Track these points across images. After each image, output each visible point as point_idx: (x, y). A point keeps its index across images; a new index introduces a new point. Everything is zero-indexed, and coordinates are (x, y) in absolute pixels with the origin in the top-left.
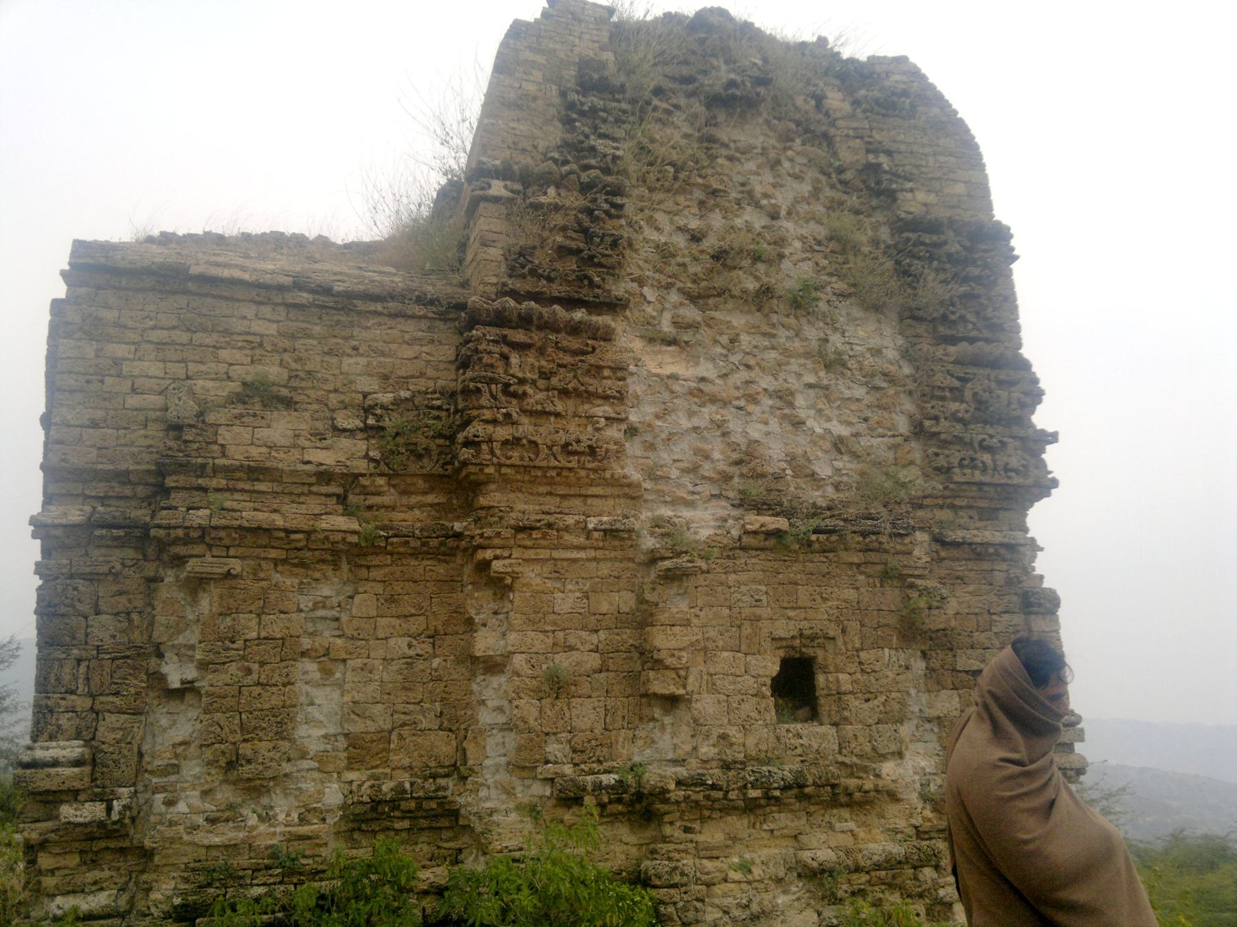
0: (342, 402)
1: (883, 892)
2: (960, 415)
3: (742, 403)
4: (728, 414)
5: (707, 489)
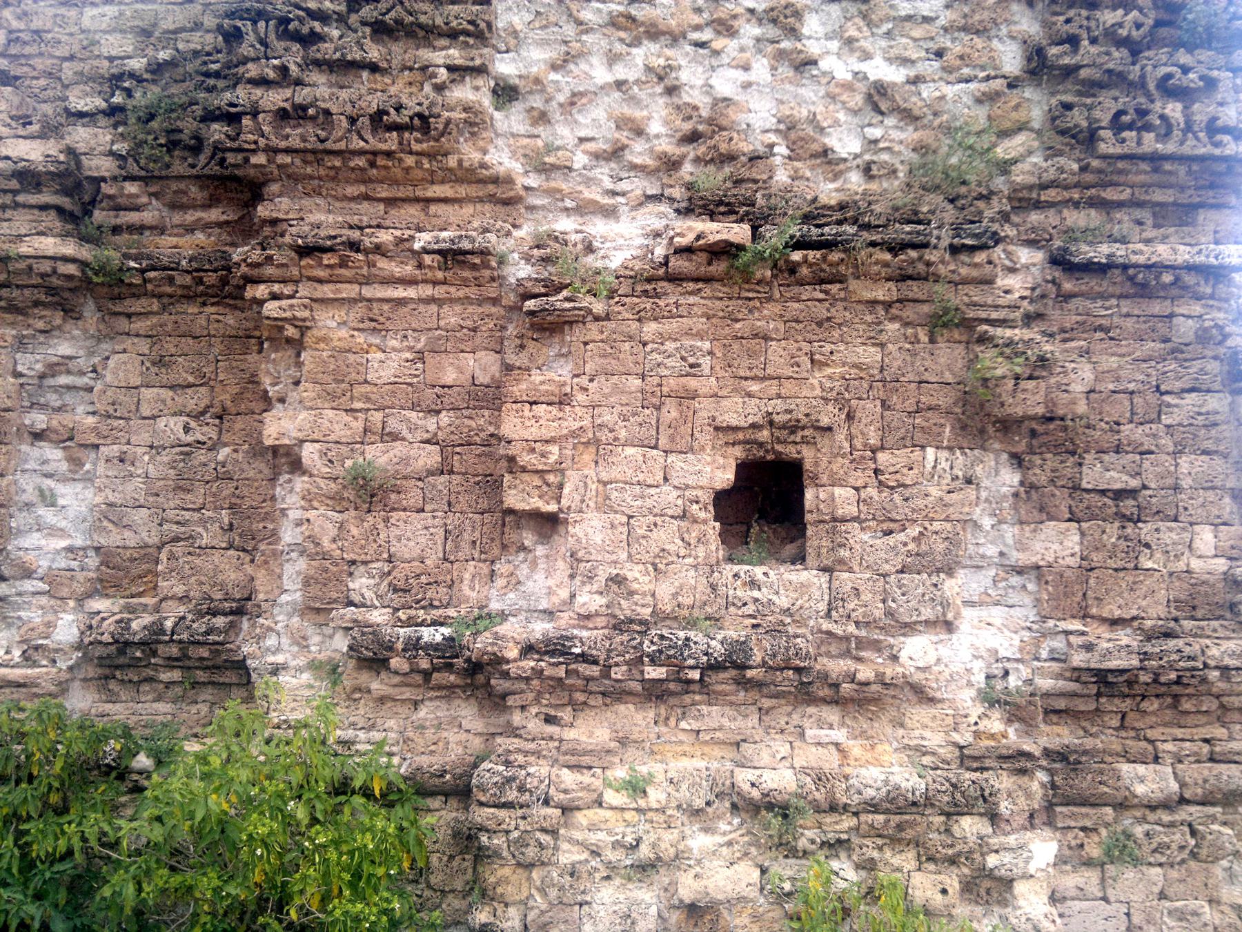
0: (82, 73)
1: (880, 849)
2: (1123, 32)
3: (706, 35)
4: (681, 55)
5: (637, 186)
